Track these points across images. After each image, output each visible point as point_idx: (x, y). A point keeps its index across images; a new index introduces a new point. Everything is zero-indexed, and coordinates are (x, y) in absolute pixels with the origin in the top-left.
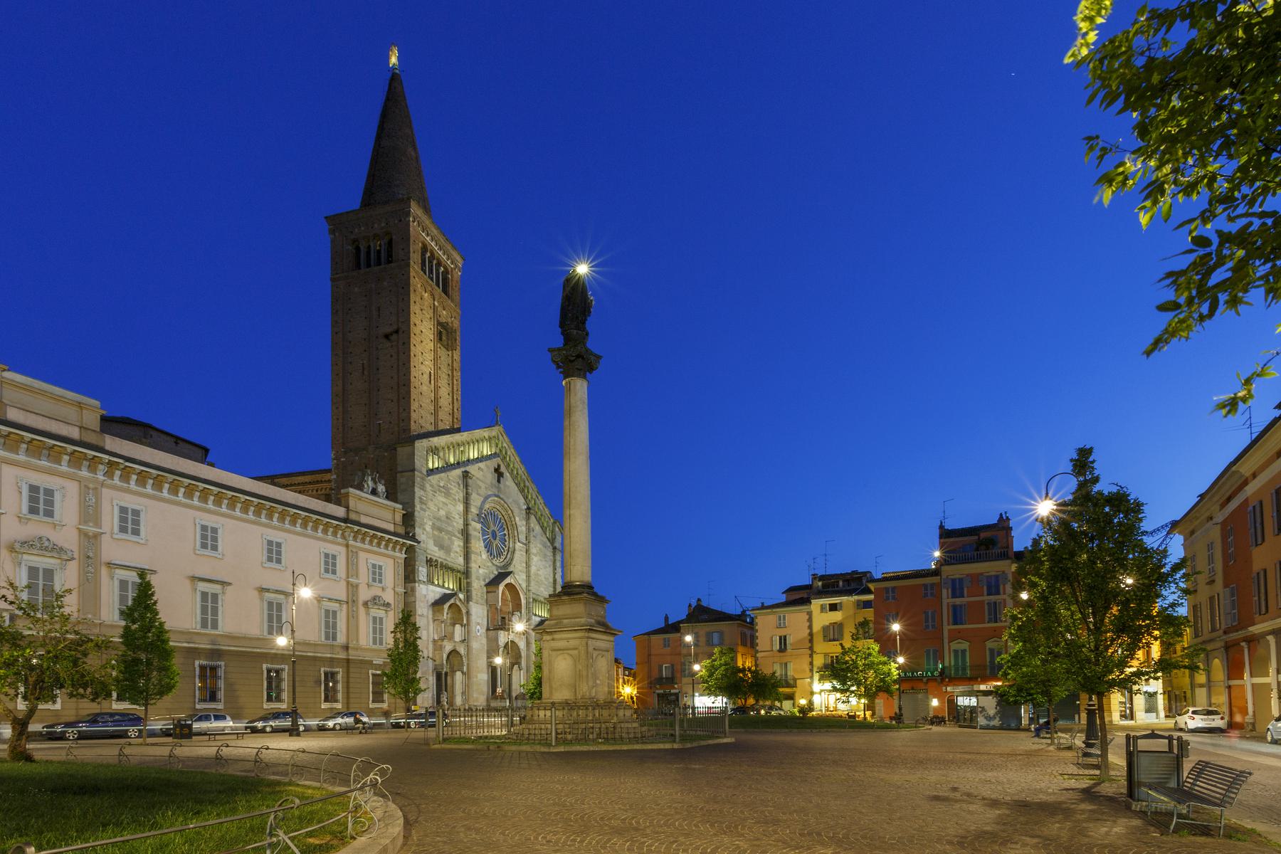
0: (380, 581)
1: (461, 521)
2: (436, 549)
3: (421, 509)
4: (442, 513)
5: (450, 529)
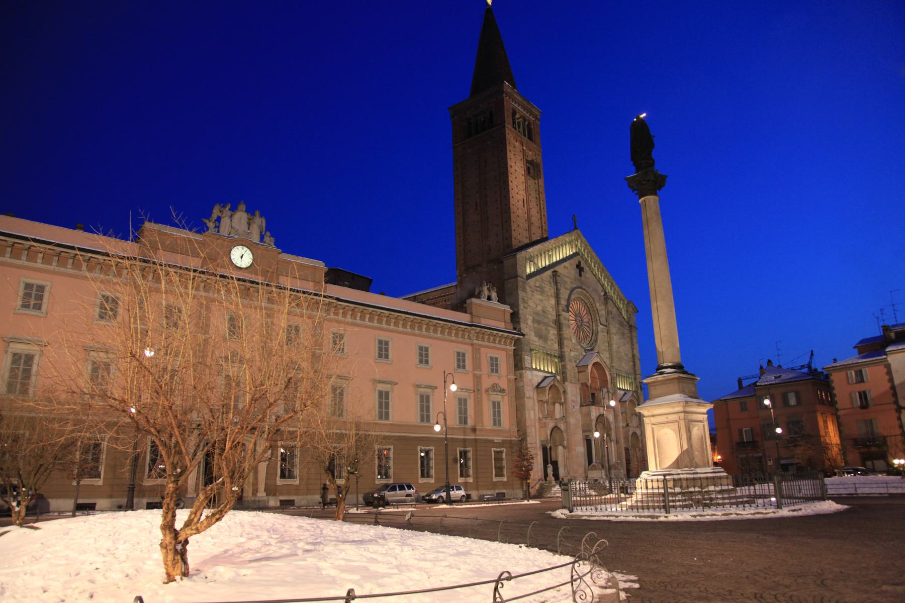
0: (497, 371)
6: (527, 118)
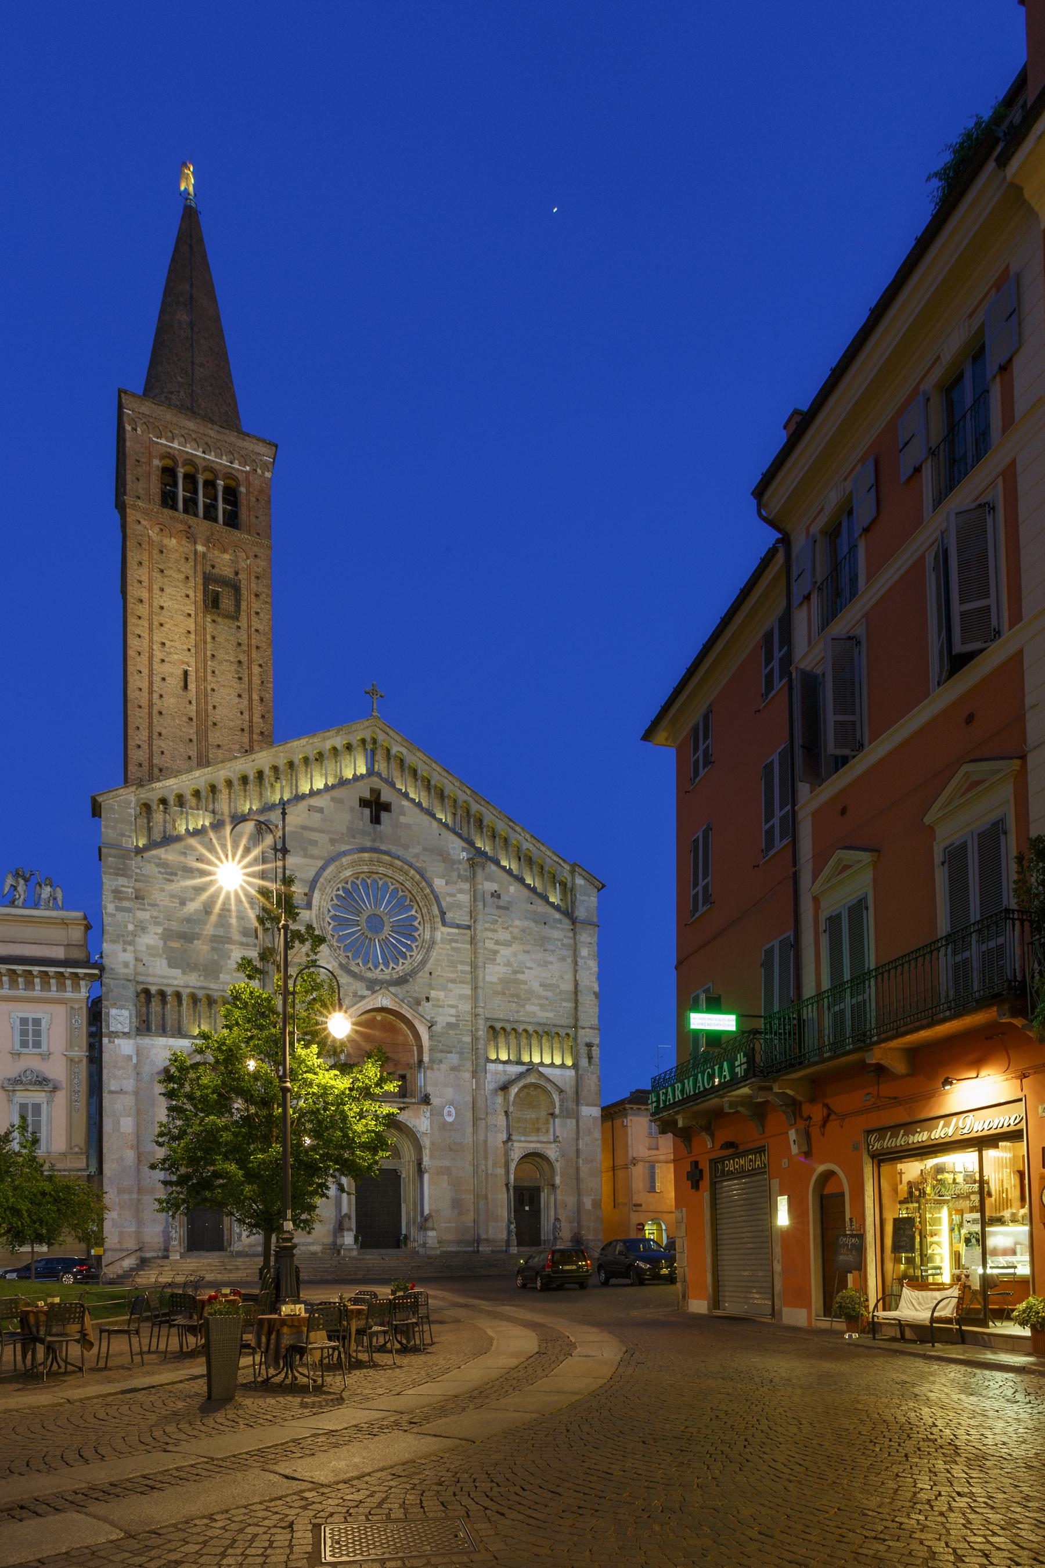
0: (37, 1044)
2: (177, 972)
6: (201, 464)
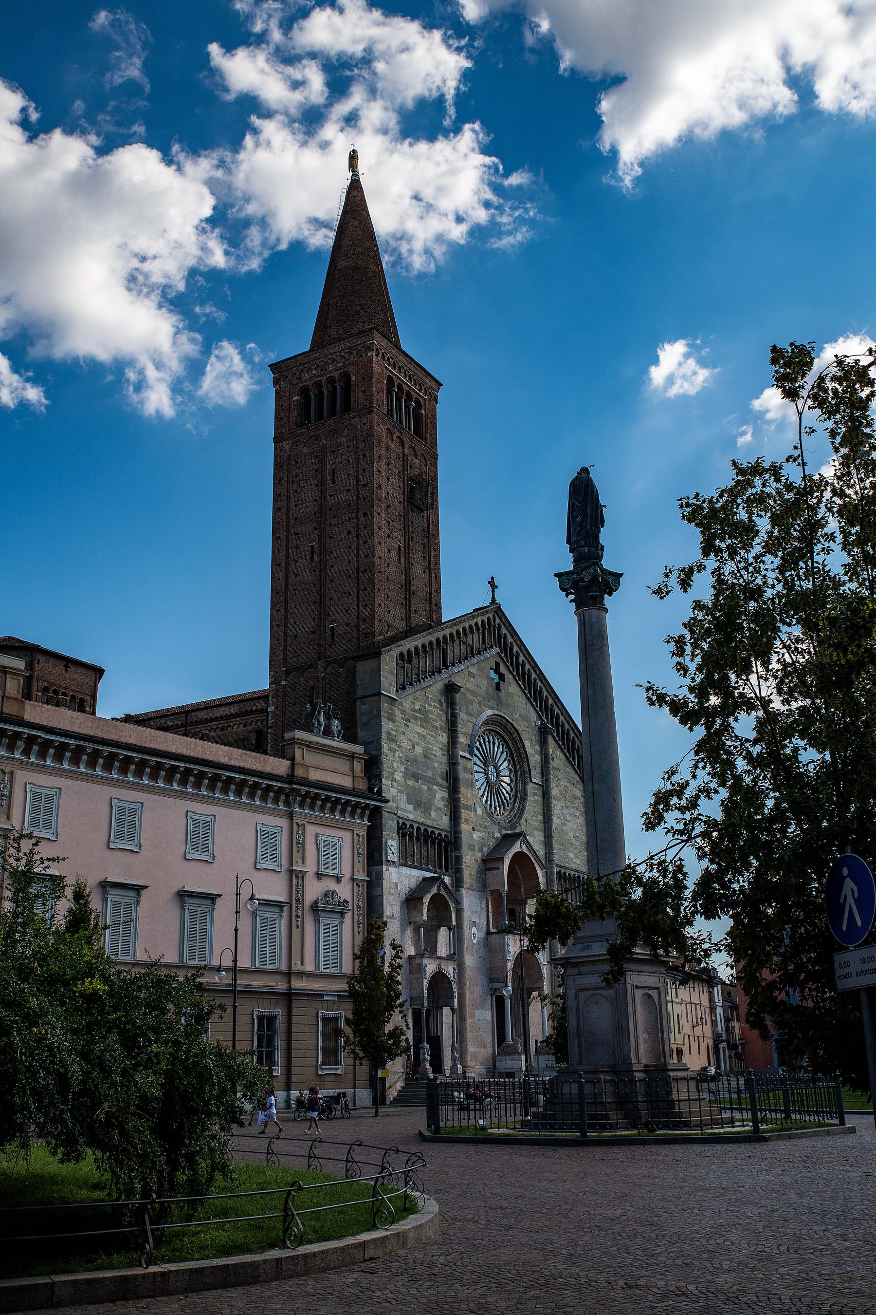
1: (445, 760)
2: (411, 807)
3: (390, 749)
4: (419, 750)
5: (429, 774)
